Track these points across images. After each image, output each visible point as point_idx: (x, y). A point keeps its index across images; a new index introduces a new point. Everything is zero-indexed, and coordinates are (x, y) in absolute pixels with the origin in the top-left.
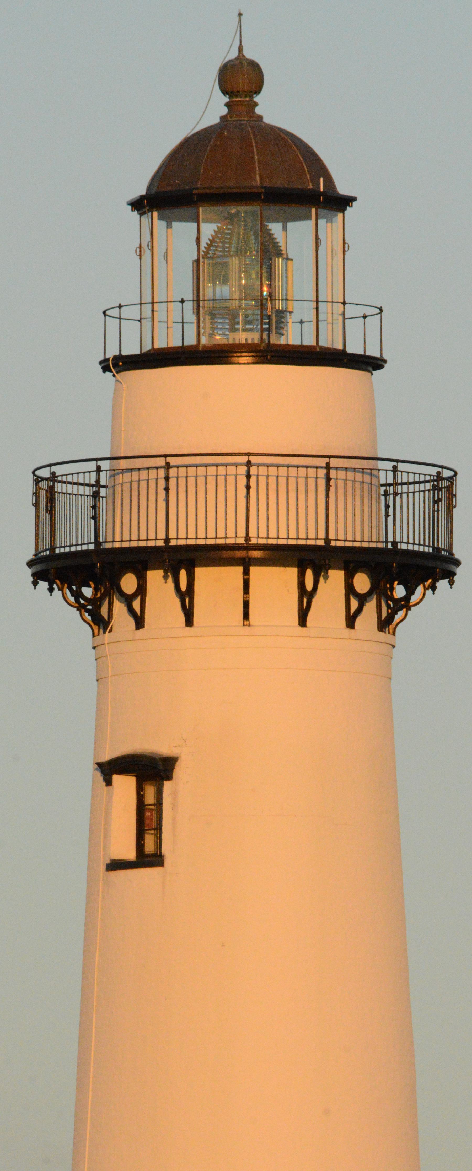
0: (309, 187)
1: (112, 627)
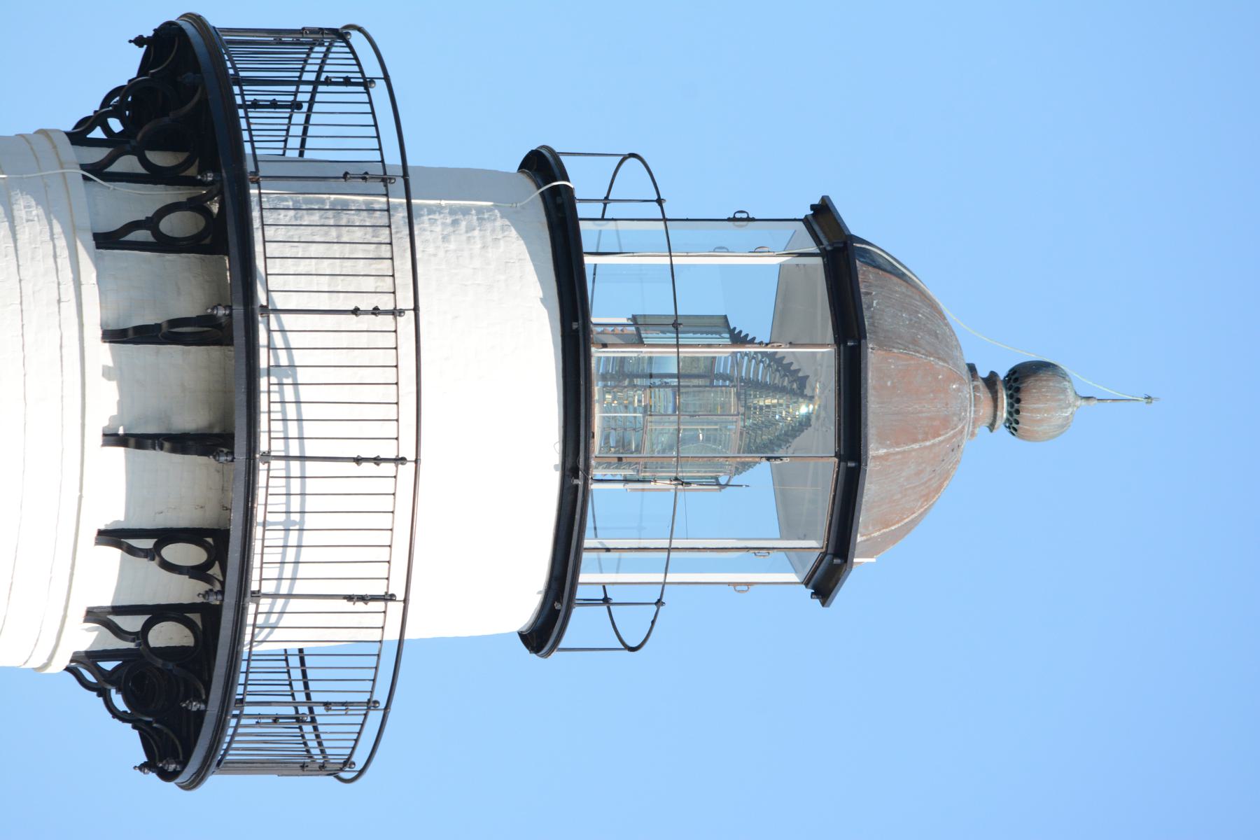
0: (859, 535)
1: (90, 179)
